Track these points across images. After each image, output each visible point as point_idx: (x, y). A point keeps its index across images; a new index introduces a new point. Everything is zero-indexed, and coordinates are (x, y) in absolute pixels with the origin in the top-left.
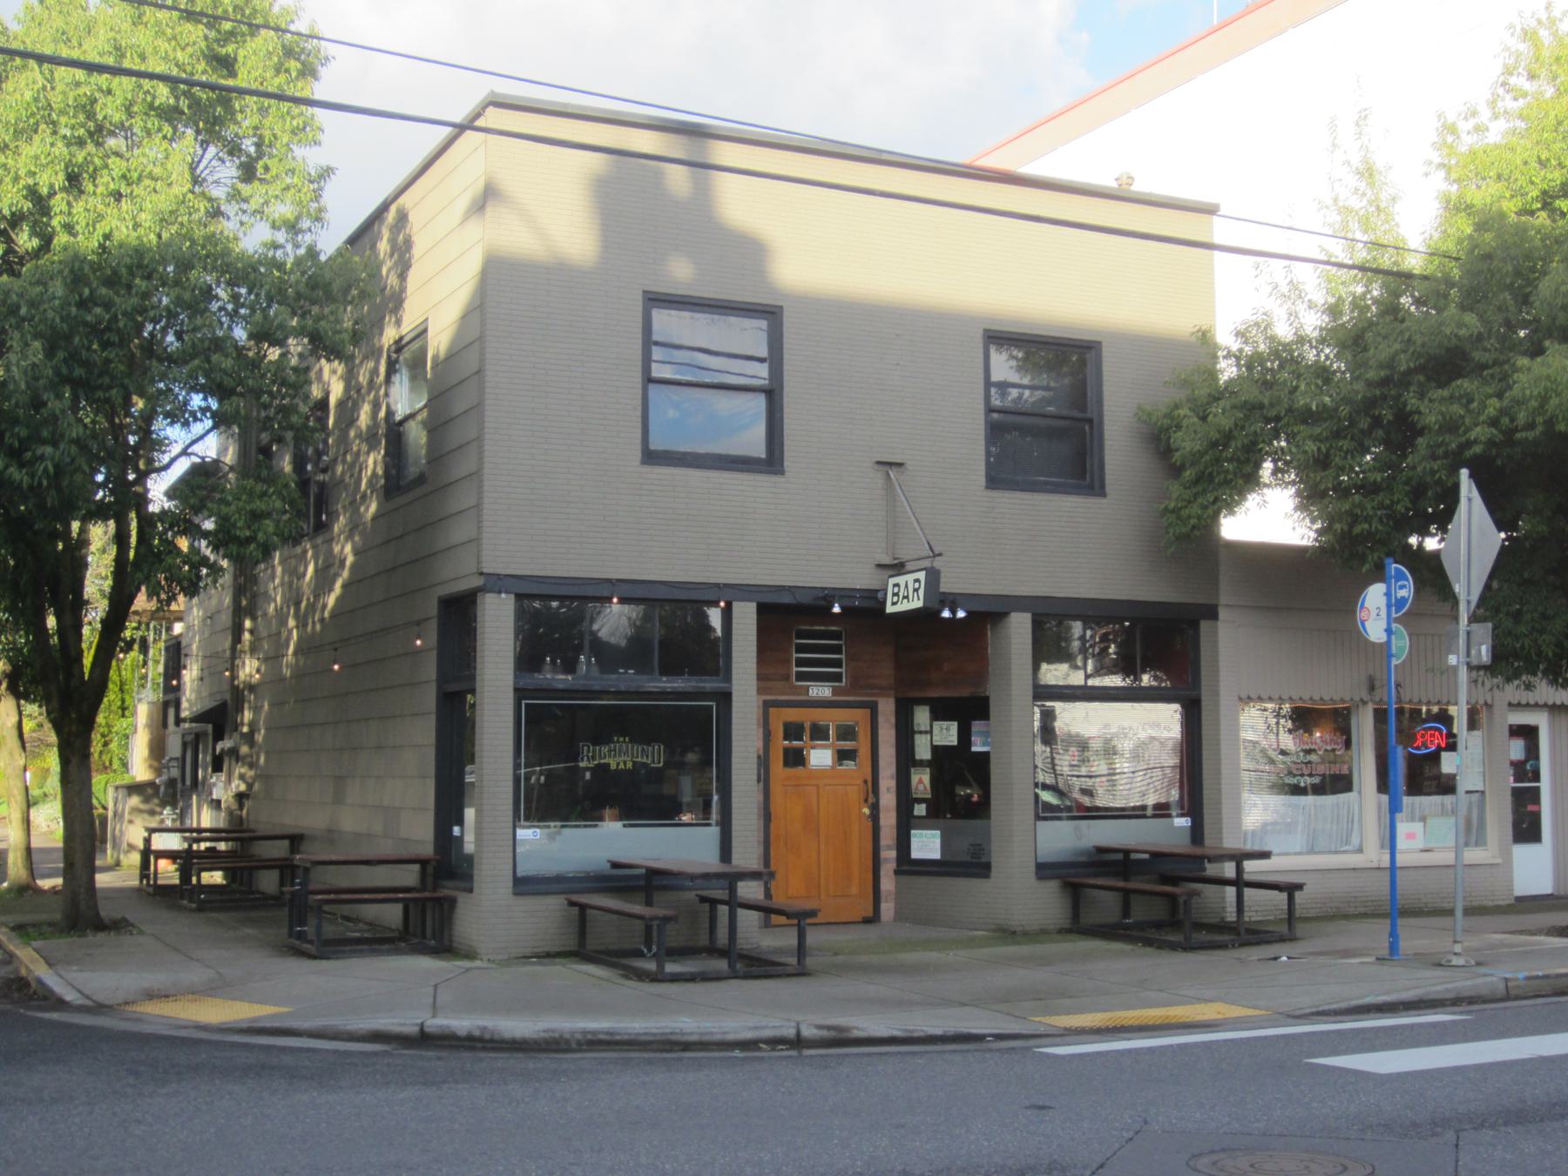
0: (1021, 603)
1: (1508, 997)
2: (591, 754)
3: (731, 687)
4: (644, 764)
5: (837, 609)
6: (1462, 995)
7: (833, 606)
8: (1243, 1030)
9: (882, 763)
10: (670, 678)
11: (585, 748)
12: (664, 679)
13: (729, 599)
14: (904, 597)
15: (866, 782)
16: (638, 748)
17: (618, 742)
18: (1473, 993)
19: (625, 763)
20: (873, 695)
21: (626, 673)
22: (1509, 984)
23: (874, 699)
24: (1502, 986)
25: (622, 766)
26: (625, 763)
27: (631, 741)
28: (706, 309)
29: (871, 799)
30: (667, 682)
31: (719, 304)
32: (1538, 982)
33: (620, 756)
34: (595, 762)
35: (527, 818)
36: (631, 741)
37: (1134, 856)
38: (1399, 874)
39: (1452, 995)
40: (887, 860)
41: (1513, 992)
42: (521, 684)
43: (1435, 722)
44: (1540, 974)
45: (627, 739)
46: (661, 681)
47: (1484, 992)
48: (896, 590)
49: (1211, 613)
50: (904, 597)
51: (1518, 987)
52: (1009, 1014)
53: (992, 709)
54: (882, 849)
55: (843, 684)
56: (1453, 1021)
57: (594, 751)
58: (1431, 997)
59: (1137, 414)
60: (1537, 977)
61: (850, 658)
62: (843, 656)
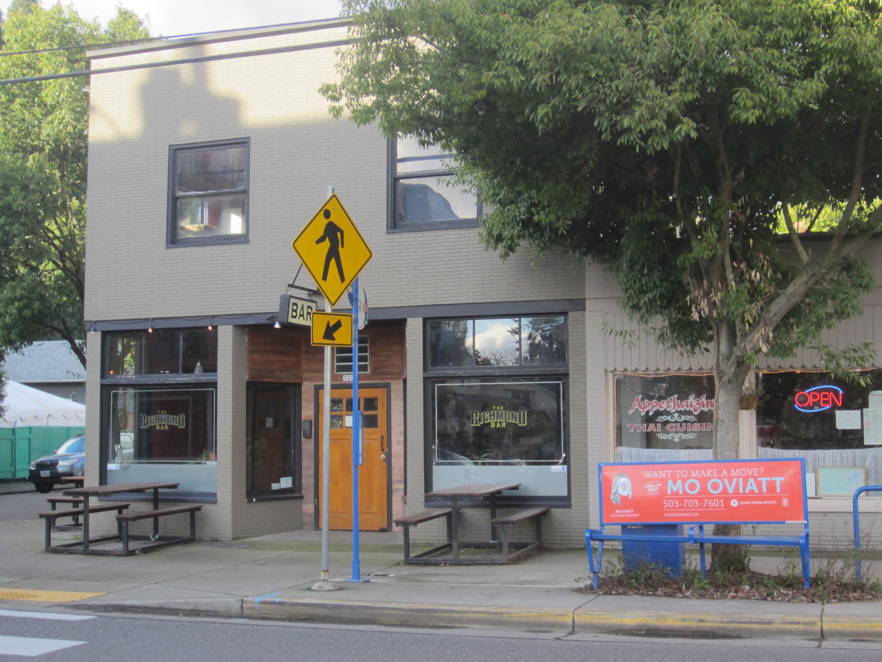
0: (414, 310)
1: (242, 615)
2: (478, 418)
3: (217, 379)
4: (515, 424)
5: (277, 326)
6: (199, 608)
7: (275, 324)
8: (15, 610)
9: (393, 425)
10: (188, 375)
11: (474, 414)
12: (184, 375)
13: (215, 325)
14: (300, 315)
15: (382, 437)
16: (509, 413)
17: (160, 413)
18: (209, 608)
19: (501, 423)
20: (387, 379)
21: (164, 373)
22: (244, 605)
23: (388, 381)
24: (237, 606)
25: (498, 425)
26: (501, 423)
27: (167, 413)
28: (235, 146)
29: (386, 449)
30: (186, 377)
31: (197, 145)
32: (273, 606)
33: (497, 419)
34: (482, 423)
35: (443, 456)
36: (504, 409)
37: (160, 490)
38: (861, 518)
39: (189, 607)
40: (397, 490)
41: (246, 612)
42: (426, 376)
43: (834, 385)
44: (277, 600)
45: (502, 408)
46: (183, 377)
47: (220, 608)
48: (295, 307)
49: (580, 305)
50: (300, 315)
51: (253, 608)
52: (860, 616)
53: (245, 386)
54: (393, 482)
55: (368, 372)
56: (81, 622)
57: (148, 419)
58: (171, 606)
59: (474, 158)
60: (274, 603)
61: (373, 354)
62: (368, 354)
